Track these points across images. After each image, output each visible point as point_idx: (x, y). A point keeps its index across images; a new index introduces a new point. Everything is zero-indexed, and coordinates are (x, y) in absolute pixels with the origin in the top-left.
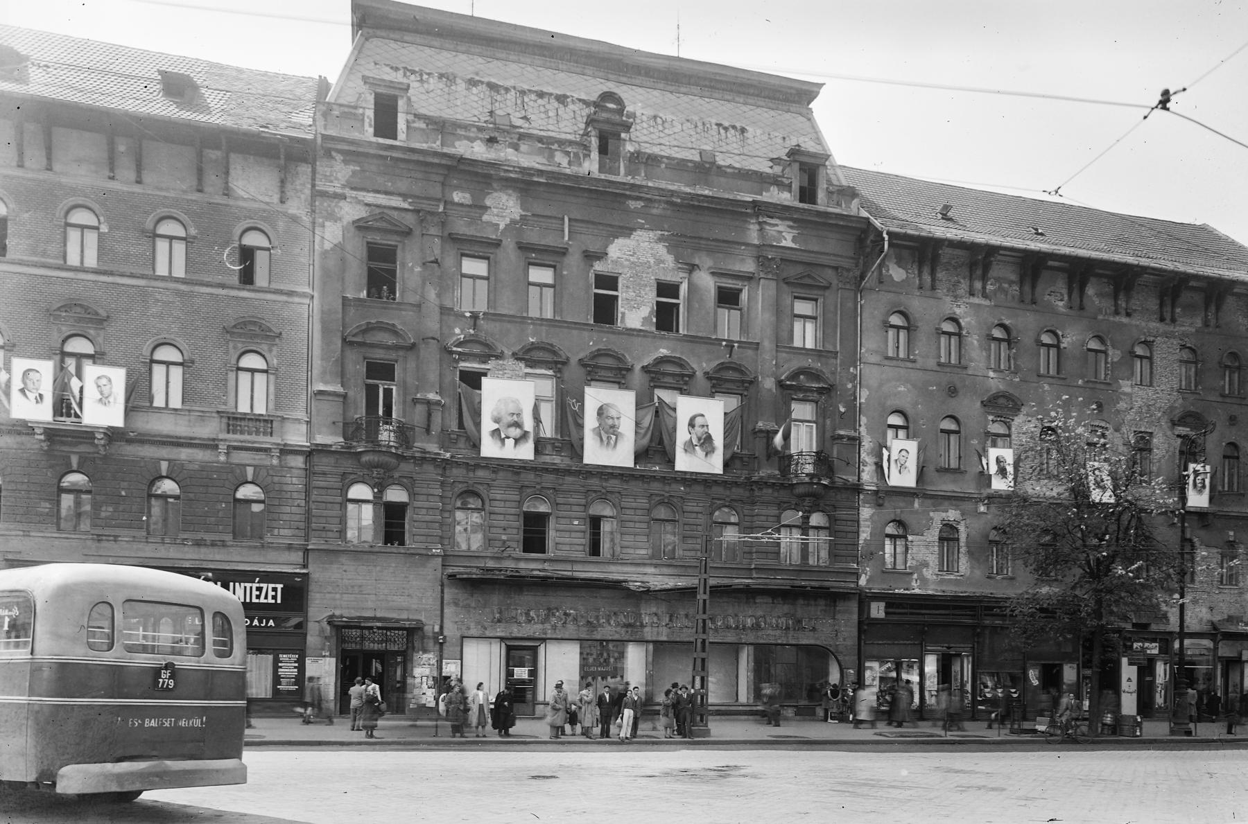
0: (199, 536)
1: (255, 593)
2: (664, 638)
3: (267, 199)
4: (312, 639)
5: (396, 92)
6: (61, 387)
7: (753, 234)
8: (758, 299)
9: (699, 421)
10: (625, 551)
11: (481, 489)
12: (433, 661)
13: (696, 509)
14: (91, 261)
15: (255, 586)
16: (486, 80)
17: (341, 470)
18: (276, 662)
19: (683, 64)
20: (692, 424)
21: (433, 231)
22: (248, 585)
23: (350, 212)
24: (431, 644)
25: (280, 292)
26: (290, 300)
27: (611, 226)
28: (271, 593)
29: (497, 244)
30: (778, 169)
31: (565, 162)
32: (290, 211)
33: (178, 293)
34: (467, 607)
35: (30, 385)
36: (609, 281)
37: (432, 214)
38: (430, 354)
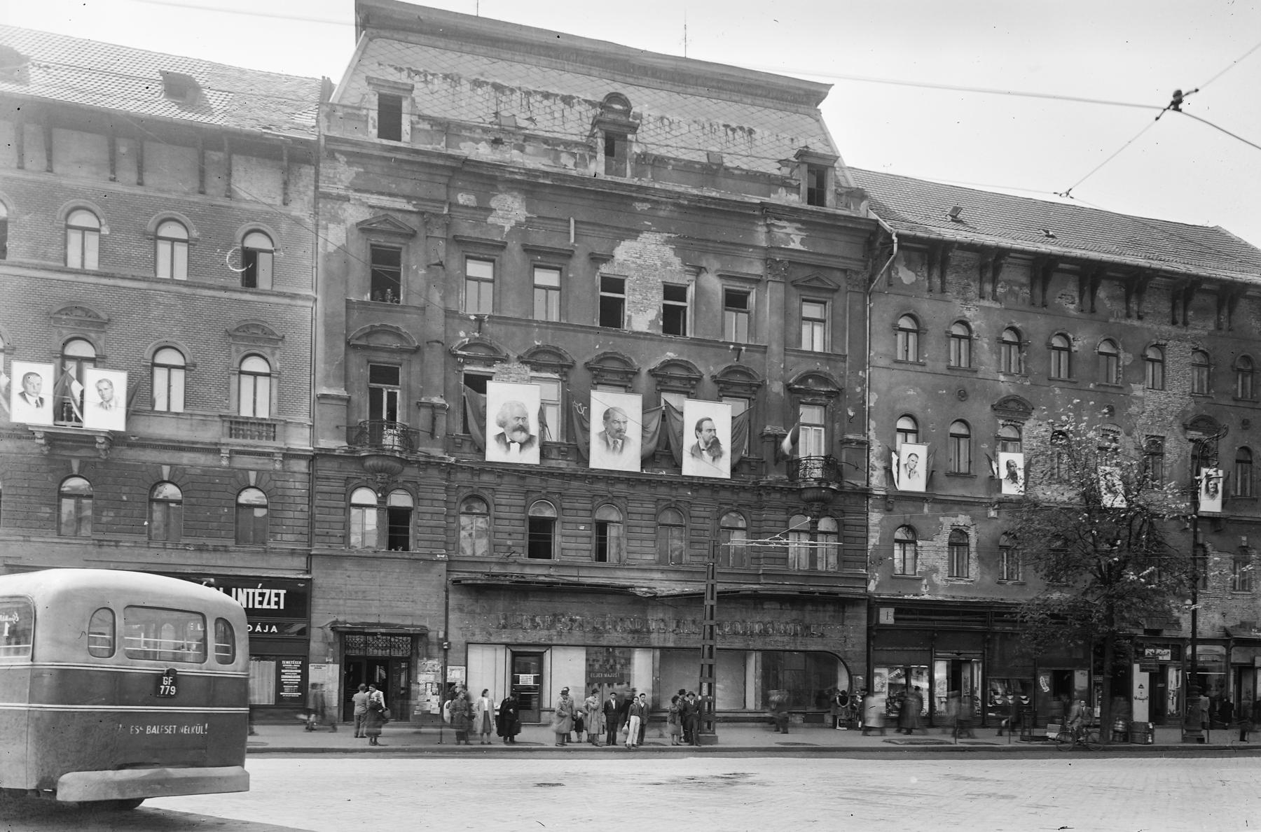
0: (201, 541)
1: (258, 599)
2: (671, 645)
3: (270, 201)
4: (316, 646)
5: (400, 93)
6: (62, 390)
7: (760, 237)
8: (766, 302)
9: (706, 425)
10: (631, 556)
11: (486, 494)
12: (438, 668)
13: (703, 514)
14: (92, 263)
15: (257, 591)
16: (491, 80)
17: (345, 475)
18: (279, 668)
20: (699, 428)
21: (437, 233)
22: (251, 591)
23: (354, 214)
24: (435, 650)
25: (283, 295)
26: (293, 302)
27: (617, 228)
28: (274, 599)
29: (502, 246)
30: (786, 171)
31: (570, 164)
32: (293, 213)
33: (180, 296)
34: (472, 613)
35: (30, 389)
36: (615, 284)
37: (436, 216)
38: (435, 357)
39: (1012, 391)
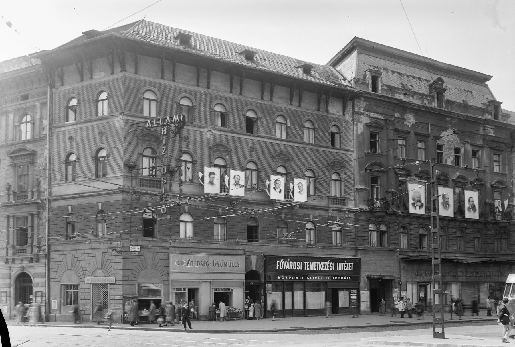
0: (324, 245)
1: (323, 266)
2: (464, 281)
3: (339, 114)
4: (362, 284)
5: (378, 75)
6: (287, 188)
8: (484, 154)
9: (471, 199)
10: (450, 248)
11: (407, 225)
12: (398, 292)
13: (470, 232)
14: (284, 137)
15: (345, 264)
17: (368, 219)
18: (350, 293)
19: (374, 55)
20: (469, 201)
21: (391, 128)
22: (343, 264)
23: (365, 120)
24: (397, 285)
25: (345, 150)
26: (348, 153)
27: (442, 127)
28: (350, 267)
29: (408, 133)
30: (485, 107)
31: (427, 104)
32: (347, 119)
33: (313, 150)
34: (407, 270)
35: (277, 186)
36: (440, 147)
37: (390, 121)
38: (392, 174)
39: (21, 113)
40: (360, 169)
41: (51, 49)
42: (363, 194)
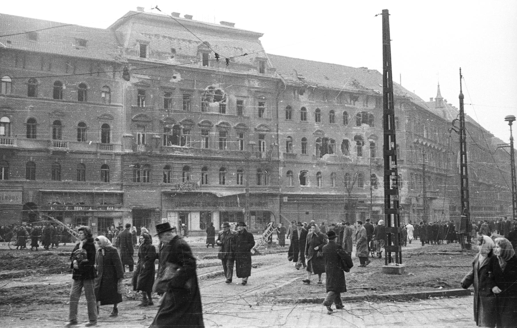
7: (246, 83)
16: (168, 36)
40: (127, 120)
41: (356, 64)
42: (129, 140)
